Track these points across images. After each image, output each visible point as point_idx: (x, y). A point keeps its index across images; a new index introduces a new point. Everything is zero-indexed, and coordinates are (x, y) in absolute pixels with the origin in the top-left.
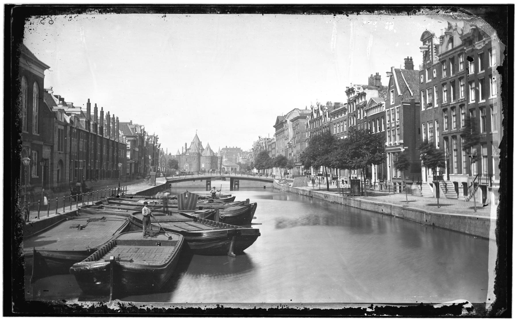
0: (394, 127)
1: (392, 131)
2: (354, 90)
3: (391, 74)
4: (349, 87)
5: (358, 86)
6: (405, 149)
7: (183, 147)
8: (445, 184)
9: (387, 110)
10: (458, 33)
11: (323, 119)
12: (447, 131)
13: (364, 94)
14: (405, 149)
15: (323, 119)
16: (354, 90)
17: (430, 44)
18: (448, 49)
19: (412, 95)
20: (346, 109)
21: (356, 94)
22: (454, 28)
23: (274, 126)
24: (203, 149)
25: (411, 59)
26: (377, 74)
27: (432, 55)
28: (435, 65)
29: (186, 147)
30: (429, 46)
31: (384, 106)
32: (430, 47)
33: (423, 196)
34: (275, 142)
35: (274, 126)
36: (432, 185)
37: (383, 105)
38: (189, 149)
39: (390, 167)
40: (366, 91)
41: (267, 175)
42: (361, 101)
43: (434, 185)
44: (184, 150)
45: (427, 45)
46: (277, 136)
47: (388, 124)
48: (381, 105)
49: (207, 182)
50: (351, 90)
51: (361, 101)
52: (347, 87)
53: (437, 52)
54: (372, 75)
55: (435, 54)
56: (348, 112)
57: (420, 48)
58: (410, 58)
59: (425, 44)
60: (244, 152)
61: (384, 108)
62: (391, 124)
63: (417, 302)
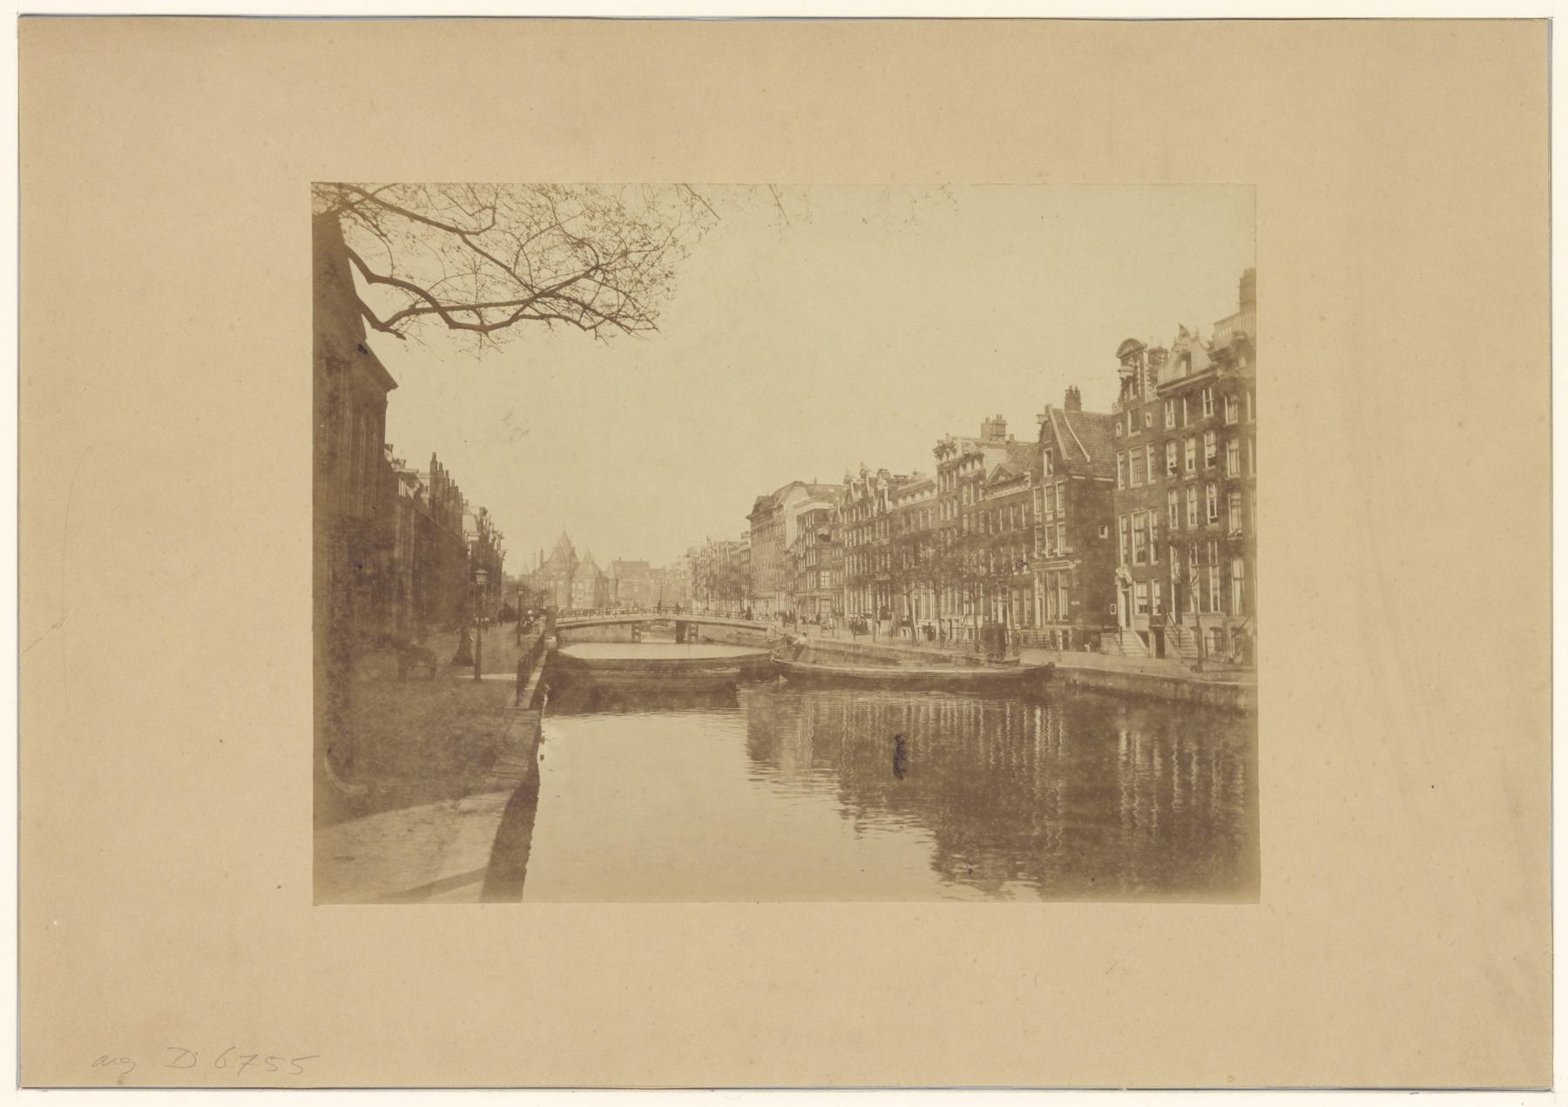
0: (1050, 522)
1: (1058, 527)
2: (955, 447)
3: (1046, 419)
4: (942, 442)
5: (963, 439)
6: (1077, 565)
7: (534, 554)
8: (1177, 633)
9: (1035, 488)
10: (1203, 347)
11: (877, 505)
12: (1216, 525)
13: (980, 457)
14: (1077, 565)
15: (874, 504)
16: (955, 447)
17: (1138, 364)
18: (1190, 370)
19: (1089, 460)
20: (934, 485)
21: (959, 454)
22: (1193, 335)
23: (748, 518)
24: (577, 564)
25: (1077, 391)
26: (999, 417)
27: (1142, 385)
28: (1149, 404)
29: (542, 558)
30: (1136, 367)
31: (1027, 481)
32: (1139, 370)
33: (1128, 655)
34: (749, 550)
35: (748, 518)
36: (1144, 636)
37: (1027, 478)
38: (547, 562)
39: (1041, 599)
40: (985, 450)
41: (728, 616)
42: (969, 470)
43: (1152, 636)
44: (538, 565)
45: (1131, 366)
46: (756, 536)
47: (1038, 516)
48: (1023, 478)
49: (633, 629)
50: (949, 447)
51: (969, 470)
52: (938, 442)
53: (1154, 380)
54: (987, 419)
55: (1149, 383)
56: (939, 489)
57: (1119, 371)
58: (1074, 389)
59: (1127, 364)
60: (657, 571)
61: (1029, 484)
62: (1044, 516)
63: (542, 757)
